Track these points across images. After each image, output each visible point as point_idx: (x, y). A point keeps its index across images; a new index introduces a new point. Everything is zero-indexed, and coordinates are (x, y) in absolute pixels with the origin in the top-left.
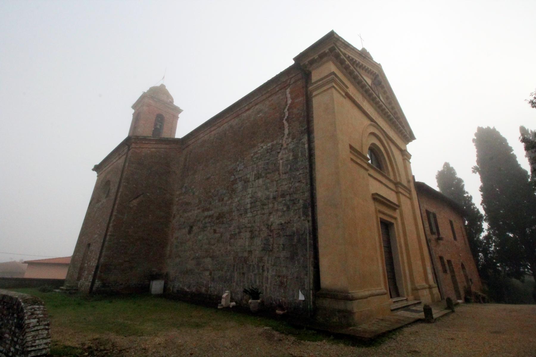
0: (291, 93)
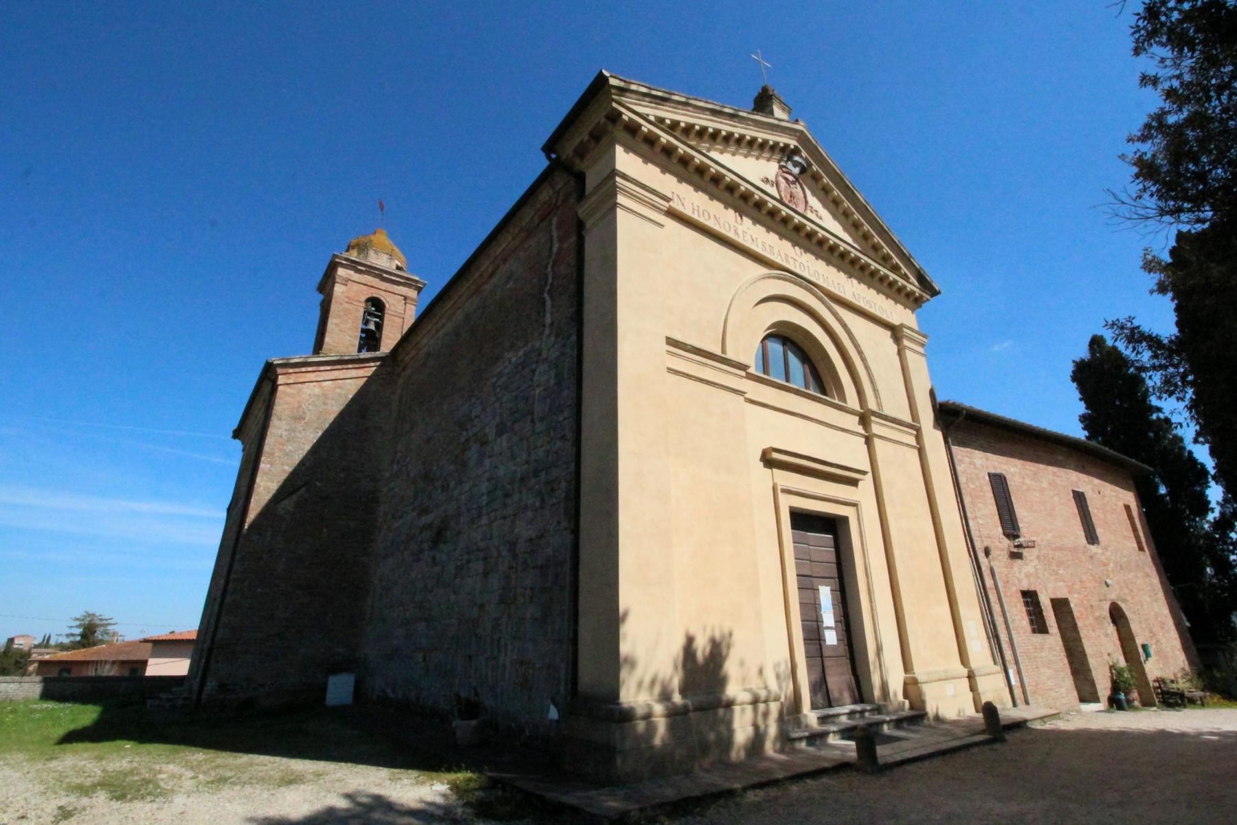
0: (559, 227)
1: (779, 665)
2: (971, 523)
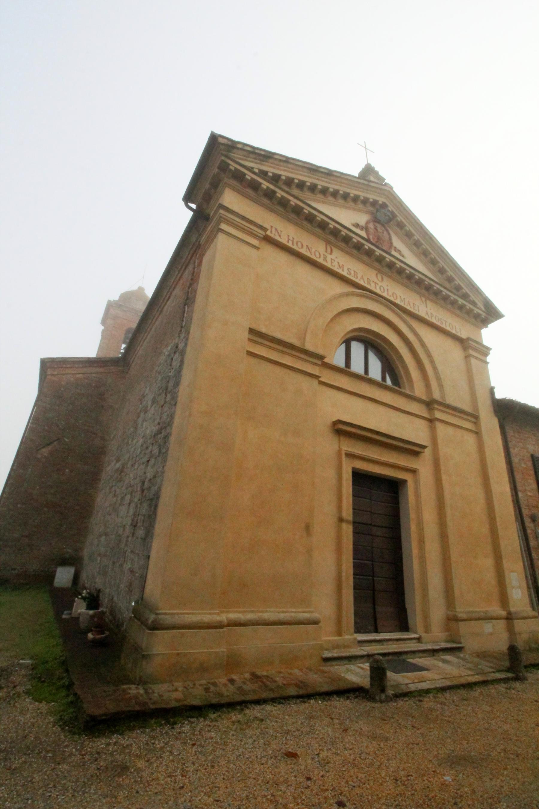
2: (520, 494)
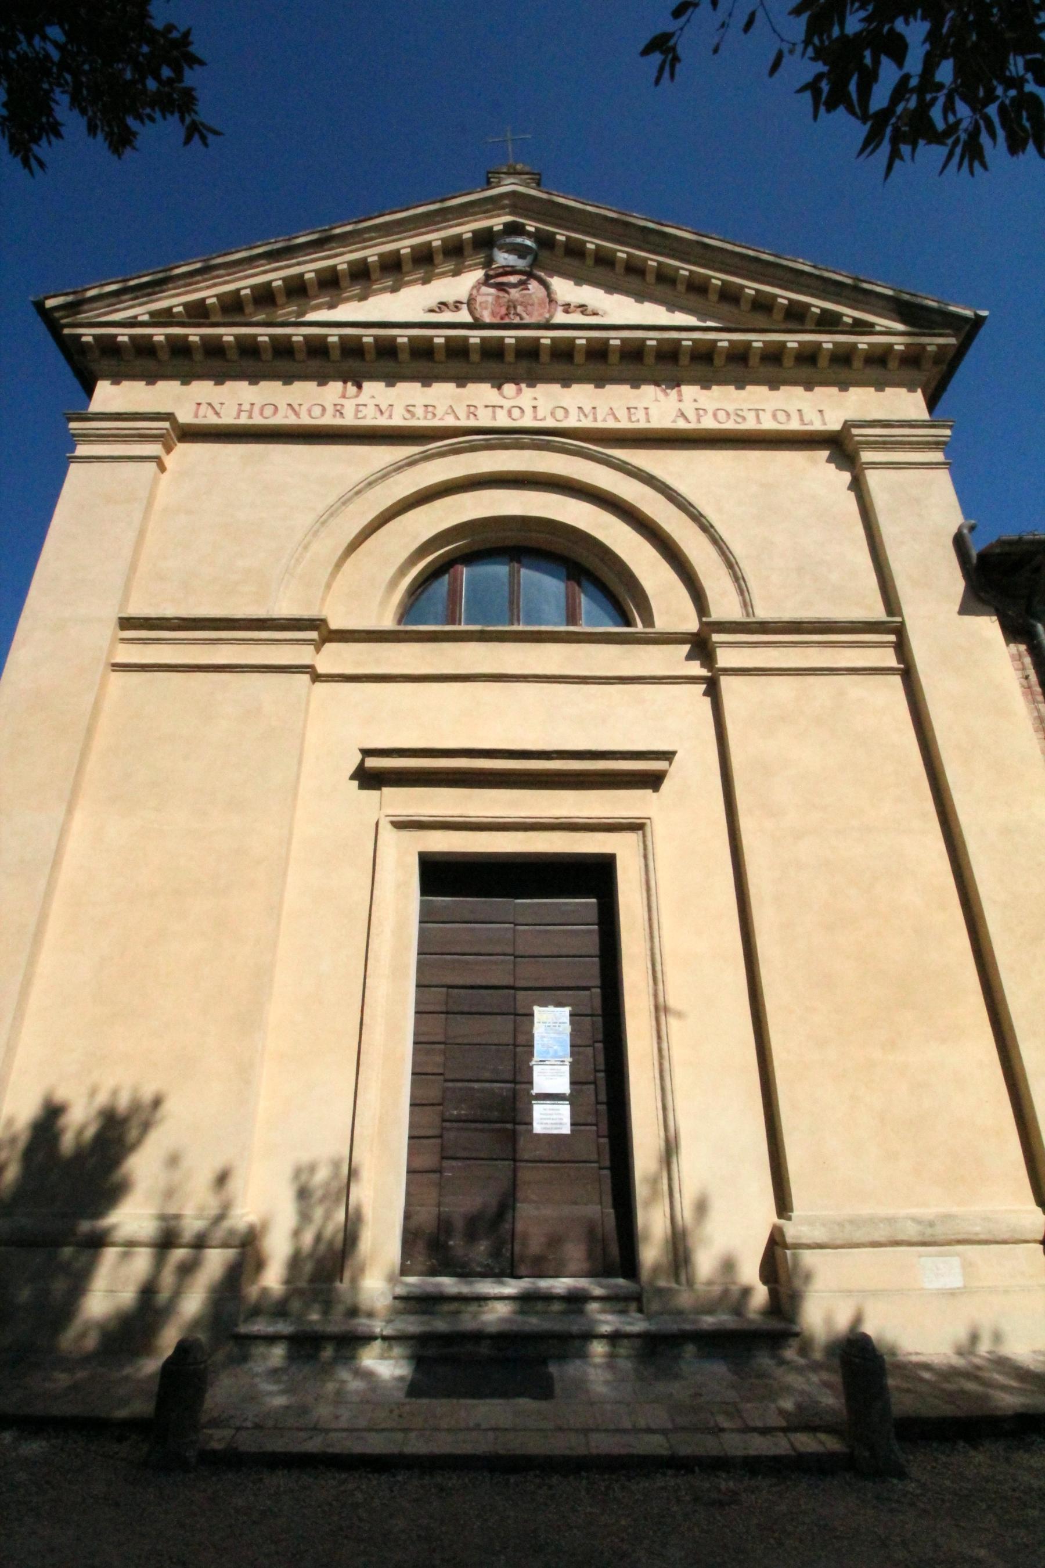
1: (312, 1168)
